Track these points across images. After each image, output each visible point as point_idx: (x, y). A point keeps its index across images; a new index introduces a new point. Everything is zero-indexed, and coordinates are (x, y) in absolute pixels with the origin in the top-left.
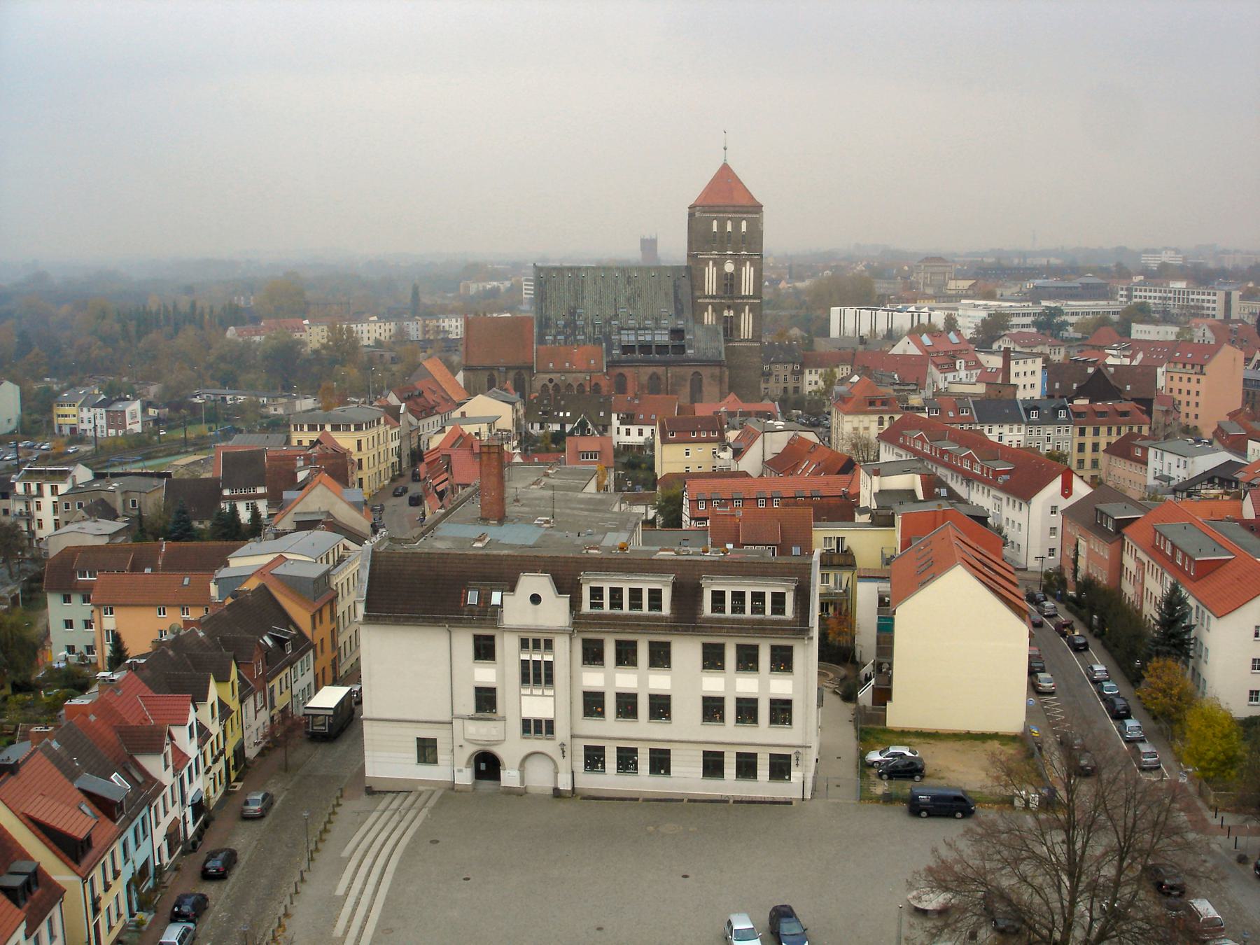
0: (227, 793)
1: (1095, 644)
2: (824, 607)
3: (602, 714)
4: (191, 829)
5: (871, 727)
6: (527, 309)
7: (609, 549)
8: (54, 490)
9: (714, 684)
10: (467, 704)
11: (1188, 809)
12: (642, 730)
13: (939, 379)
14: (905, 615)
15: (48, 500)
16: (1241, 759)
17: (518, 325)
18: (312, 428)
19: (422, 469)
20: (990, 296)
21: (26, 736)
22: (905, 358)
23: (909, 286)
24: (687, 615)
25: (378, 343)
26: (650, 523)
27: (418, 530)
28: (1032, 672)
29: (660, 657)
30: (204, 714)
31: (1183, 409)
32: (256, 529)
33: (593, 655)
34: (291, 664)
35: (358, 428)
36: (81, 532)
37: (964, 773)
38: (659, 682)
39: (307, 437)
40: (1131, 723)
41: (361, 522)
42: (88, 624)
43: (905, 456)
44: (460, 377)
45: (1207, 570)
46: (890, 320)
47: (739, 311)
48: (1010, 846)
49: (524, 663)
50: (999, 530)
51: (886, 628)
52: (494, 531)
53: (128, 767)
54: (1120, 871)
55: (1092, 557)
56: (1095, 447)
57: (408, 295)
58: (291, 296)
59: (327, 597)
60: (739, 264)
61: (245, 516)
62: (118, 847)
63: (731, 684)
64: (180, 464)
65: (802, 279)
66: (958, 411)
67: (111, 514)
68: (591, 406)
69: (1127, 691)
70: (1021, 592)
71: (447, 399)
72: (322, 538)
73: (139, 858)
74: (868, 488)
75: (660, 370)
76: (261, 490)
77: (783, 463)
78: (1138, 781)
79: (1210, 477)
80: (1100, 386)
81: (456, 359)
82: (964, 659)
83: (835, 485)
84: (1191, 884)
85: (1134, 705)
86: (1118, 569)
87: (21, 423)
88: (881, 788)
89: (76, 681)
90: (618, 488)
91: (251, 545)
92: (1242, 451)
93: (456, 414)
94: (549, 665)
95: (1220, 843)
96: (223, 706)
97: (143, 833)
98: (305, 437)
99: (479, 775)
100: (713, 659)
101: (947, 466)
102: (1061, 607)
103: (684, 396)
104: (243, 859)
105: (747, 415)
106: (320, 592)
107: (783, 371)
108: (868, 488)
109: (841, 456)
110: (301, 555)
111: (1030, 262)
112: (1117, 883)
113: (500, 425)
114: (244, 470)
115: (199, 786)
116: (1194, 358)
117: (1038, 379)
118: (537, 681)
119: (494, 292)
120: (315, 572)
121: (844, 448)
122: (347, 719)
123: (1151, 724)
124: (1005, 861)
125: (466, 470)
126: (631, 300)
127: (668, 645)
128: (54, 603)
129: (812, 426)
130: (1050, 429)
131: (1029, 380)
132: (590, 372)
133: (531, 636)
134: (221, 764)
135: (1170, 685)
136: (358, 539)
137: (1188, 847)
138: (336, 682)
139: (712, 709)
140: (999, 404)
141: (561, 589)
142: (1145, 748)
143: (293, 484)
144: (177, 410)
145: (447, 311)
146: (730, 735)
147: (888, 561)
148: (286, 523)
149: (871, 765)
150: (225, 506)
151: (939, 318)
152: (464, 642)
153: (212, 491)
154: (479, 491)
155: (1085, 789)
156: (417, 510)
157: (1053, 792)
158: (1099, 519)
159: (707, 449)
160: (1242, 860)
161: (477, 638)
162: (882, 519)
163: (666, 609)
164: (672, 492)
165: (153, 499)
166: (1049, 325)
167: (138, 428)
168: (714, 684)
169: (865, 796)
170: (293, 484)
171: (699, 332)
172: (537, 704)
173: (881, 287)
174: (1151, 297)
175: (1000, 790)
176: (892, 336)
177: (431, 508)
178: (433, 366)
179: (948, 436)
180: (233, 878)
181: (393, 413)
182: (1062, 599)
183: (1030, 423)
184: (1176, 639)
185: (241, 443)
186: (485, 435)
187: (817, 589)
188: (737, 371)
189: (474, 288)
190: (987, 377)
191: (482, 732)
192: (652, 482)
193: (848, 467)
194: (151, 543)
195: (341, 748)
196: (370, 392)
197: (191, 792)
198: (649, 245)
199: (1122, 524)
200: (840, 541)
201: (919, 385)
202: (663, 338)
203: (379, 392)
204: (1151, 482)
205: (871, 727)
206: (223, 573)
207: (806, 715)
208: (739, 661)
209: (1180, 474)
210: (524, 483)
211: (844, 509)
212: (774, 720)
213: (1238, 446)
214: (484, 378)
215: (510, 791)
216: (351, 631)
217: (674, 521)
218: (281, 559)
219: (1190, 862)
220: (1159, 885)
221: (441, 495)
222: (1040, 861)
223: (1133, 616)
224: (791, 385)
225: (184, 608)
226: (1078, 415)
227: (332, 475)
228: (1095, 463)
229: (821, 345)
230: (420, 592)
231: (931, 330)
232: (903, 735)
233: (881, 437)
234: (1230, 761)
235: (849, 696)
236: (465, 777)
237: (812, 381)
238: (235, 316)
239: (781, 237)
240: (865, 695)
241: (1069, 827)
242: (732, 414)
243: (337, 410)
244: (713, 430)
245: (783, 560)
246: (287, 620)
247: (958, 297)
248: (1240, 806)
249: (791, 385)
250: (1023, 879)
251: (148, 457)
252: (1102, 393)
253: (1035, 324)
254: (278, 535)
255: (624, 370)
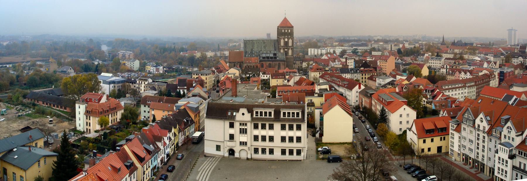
0: (174, 153)
1: (367, 121)
2: (308, 115)
3: (258, 140)
4: (166, 160)
5: (319, 142)
6: (242, 49)
7: (260, 103)
8: (144, 83)
9: (284, 133)
10: (228, 138)
11: (389, 156)
12: (267, 144)
13: (332, 64)
14: (326, 117)
15: (143, 85)
16: (398, 143)
17: (240, 53)
18: (197, 75)
19: (219, 84)
20: (342, 46)
21: (134, 134)
22: (325, 59)
23: (325, 44)
24: (277, 118)
25: (211, 57)
26: (269, 97)
27: (218, 98)
28: (354, 128)
29: (271, 127)
30: (170, 135)
31: (383, 69)
32: (184, 96)
33: (256, 127)
34: (190, 126)
35: (206, 75)
36: (149, 93)
37: (340, 152)
38: (271, 133)
39: (195, 76)
40: (375, 138)
41: (206, 96)
42: (149, 112)
43: (325, 81)
44: (228, 64)
45: (389, 103)
46: (321, 51)
47: (288, 49)
48: (350, 168)
49: (240, 129)
50: (346, 97)
51: (322, 120)
52: (234, 99)
53: (154, 144)
54: (375, 171)
55: (365, 102)
56: (365, 78)
57: (218, 46)
58: (194, 46)
59: (198, 112)
60: (288, 39)
61: (182, 93)
62: (150, 161)
63: (288, 133)
64: (169, 80)
65: (302, 42)
66: (336, 71)
67: (155, 90)
68: (256, 70)
69: (374, 131)
70: (351, 110)
71: (225, 69)
72: (198, 99)
73: (154, 164)
74: (317, 88)
75: (271, 63)
76: (185, 87)
77: (298, 83)
78: (377, 151)
79: (389, 83)
80: (366, 65)
81: (227, 60)
82: (339, 126)
83: (310, 88)
84: (390, 173)
85: (376, 134)
86: (371, 104)
87: (139, 68)
88: (321, 156)
89: (145, 124)
90: (262, 89)
91: (183, 99)
92: (395, 78)
93: (227, 72)
94: (246, 129)
95: (396, 163)
96: (175, 133)
97: (156, 159)
98: (195, 76)
99: (230, 154)
100: (283, 128)
101: (334, 83)
102: (359, 113)
103: (277, 69)
104: (176, 168)
105: (290, 72)
106: (197, 111)
107: (298, 62)
108: (317, 88)
109: (311, 81)
110: (193, 102)
111: (351, 39)
112: (374, 174)
113: (236, 75)
114: (182, 83)
115: (168, 150)
116: (385, 59)
117: (353, 64)
118: (243, 133)
119: (235, 46)
120: (196, 106)
121: (312, 80)
122: (201, 139)
123: (379, 138)
124: (350, 172)
125: (229, 85)
126: (265, 47)
127: (273, 124)
128: (142, 106)
129: (305, 75)
130: (356, 74)
131: (351, 64)
132: (255, 63)
133: (242, 123)
134: (173, 146)
135: (383, 129)
136: (205, 99)
137: (389, 164)
138: (199, 131)
139: (283, 139)
140: (345, 69)
141: (249, 112)
142: (378, 143)
143: (192, 86)
144: (170, 69)
145: (225, 50)
146: (287, 145)
147: (322, 105)
148: (190, 95)
149: (319, 151)
150: (178, 90)
151: (332, 51)
152: (227, 123)
153: (174, 87)
154: (231, 90)
155: (366, 154)
156: (218, 94)
157: (359, 155)
158: (366, 93)
159: (282, 80)
160: (401, 166)
161: (230, 123)
162: (320, 95)
163: (273, 116)
164: (274, 90)
165: (164, 87)
166: (355, 52)
167: (162, 72)
168: (284, 133)
169: (318, 158)
170: (192, 86)
171: (280, 54)
172: (243, 138)
173: (319, 44)
174: (376, 46)
175: (347, 155)
176: (322, 55)
177: (221, 94)
178: (222, 62)
179: (334, 76)
180: (174, 172)
181: (214, 72)
182: (359, 111)
183: (352, 73)
184: (384, 118)
185: (182, 77)
186: (233, 77)
187: (306, 111)
188: (288, 63)
189: (231, 45)
190: (342, 63)
191: (231, 144)
192: (269, 88)
193: (313, 84)
194: (162, 97)
195: (199, 145)
196: (209, 67)
197: (166, 152)
198: (269, 35)
199: (371, 94)
200: (311, 100)
201: (328, 65)
202: (272, 55)
203: (211, 67)
204: (377, 85)
205: (319, 142)
206: (177, 105)
207: (304, 140)
208: (289, 128)
209: (383, 83)
210: (241, 88)
211: (312, 93)
212: (297, 142)
213: (394, 77)
214: (233, 64)
215: (237, 158)
216: (203, 120)
217: (274, 96)
218: (189, 103)
219: (390, 168)
220: (383, 174)
221: (223, 90)
222: (357, 171)
223: (374, 114)
224: (300, 66)
225: (168, 111)
226: (361, 71)
227: (201, 85)
228: (365, 82)
229: (306, 57)
230: (219, 112)
231: (330, 53)
232: (326, 144)
233: (320, 77)
234: (396, 144)
235: (314, 135)
236: (227, 155)
237: (305, 65)
238: (182, 50)
239: (297, 34)
240: (317, 135)
241: (363, 163)
242: (287, 72)
243: (202, 71)
244: (282, 76)
245: (299, 105)
246: (190, 116)
247: (336, 46)
248: (400, 154)
249: (300, 66)
250: (354, 175)
251: (163, 78)
252: (367, 66)
253: (352, 52)
254: (188, 97)
255: (264, 63)
